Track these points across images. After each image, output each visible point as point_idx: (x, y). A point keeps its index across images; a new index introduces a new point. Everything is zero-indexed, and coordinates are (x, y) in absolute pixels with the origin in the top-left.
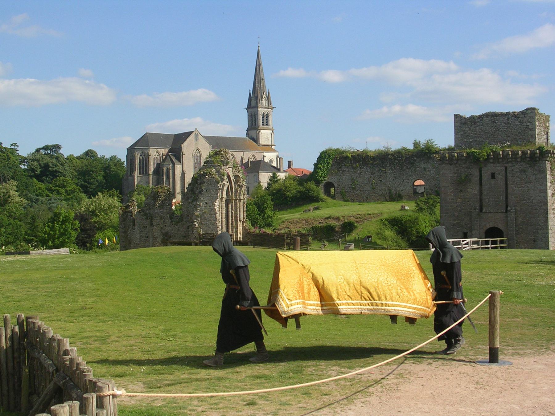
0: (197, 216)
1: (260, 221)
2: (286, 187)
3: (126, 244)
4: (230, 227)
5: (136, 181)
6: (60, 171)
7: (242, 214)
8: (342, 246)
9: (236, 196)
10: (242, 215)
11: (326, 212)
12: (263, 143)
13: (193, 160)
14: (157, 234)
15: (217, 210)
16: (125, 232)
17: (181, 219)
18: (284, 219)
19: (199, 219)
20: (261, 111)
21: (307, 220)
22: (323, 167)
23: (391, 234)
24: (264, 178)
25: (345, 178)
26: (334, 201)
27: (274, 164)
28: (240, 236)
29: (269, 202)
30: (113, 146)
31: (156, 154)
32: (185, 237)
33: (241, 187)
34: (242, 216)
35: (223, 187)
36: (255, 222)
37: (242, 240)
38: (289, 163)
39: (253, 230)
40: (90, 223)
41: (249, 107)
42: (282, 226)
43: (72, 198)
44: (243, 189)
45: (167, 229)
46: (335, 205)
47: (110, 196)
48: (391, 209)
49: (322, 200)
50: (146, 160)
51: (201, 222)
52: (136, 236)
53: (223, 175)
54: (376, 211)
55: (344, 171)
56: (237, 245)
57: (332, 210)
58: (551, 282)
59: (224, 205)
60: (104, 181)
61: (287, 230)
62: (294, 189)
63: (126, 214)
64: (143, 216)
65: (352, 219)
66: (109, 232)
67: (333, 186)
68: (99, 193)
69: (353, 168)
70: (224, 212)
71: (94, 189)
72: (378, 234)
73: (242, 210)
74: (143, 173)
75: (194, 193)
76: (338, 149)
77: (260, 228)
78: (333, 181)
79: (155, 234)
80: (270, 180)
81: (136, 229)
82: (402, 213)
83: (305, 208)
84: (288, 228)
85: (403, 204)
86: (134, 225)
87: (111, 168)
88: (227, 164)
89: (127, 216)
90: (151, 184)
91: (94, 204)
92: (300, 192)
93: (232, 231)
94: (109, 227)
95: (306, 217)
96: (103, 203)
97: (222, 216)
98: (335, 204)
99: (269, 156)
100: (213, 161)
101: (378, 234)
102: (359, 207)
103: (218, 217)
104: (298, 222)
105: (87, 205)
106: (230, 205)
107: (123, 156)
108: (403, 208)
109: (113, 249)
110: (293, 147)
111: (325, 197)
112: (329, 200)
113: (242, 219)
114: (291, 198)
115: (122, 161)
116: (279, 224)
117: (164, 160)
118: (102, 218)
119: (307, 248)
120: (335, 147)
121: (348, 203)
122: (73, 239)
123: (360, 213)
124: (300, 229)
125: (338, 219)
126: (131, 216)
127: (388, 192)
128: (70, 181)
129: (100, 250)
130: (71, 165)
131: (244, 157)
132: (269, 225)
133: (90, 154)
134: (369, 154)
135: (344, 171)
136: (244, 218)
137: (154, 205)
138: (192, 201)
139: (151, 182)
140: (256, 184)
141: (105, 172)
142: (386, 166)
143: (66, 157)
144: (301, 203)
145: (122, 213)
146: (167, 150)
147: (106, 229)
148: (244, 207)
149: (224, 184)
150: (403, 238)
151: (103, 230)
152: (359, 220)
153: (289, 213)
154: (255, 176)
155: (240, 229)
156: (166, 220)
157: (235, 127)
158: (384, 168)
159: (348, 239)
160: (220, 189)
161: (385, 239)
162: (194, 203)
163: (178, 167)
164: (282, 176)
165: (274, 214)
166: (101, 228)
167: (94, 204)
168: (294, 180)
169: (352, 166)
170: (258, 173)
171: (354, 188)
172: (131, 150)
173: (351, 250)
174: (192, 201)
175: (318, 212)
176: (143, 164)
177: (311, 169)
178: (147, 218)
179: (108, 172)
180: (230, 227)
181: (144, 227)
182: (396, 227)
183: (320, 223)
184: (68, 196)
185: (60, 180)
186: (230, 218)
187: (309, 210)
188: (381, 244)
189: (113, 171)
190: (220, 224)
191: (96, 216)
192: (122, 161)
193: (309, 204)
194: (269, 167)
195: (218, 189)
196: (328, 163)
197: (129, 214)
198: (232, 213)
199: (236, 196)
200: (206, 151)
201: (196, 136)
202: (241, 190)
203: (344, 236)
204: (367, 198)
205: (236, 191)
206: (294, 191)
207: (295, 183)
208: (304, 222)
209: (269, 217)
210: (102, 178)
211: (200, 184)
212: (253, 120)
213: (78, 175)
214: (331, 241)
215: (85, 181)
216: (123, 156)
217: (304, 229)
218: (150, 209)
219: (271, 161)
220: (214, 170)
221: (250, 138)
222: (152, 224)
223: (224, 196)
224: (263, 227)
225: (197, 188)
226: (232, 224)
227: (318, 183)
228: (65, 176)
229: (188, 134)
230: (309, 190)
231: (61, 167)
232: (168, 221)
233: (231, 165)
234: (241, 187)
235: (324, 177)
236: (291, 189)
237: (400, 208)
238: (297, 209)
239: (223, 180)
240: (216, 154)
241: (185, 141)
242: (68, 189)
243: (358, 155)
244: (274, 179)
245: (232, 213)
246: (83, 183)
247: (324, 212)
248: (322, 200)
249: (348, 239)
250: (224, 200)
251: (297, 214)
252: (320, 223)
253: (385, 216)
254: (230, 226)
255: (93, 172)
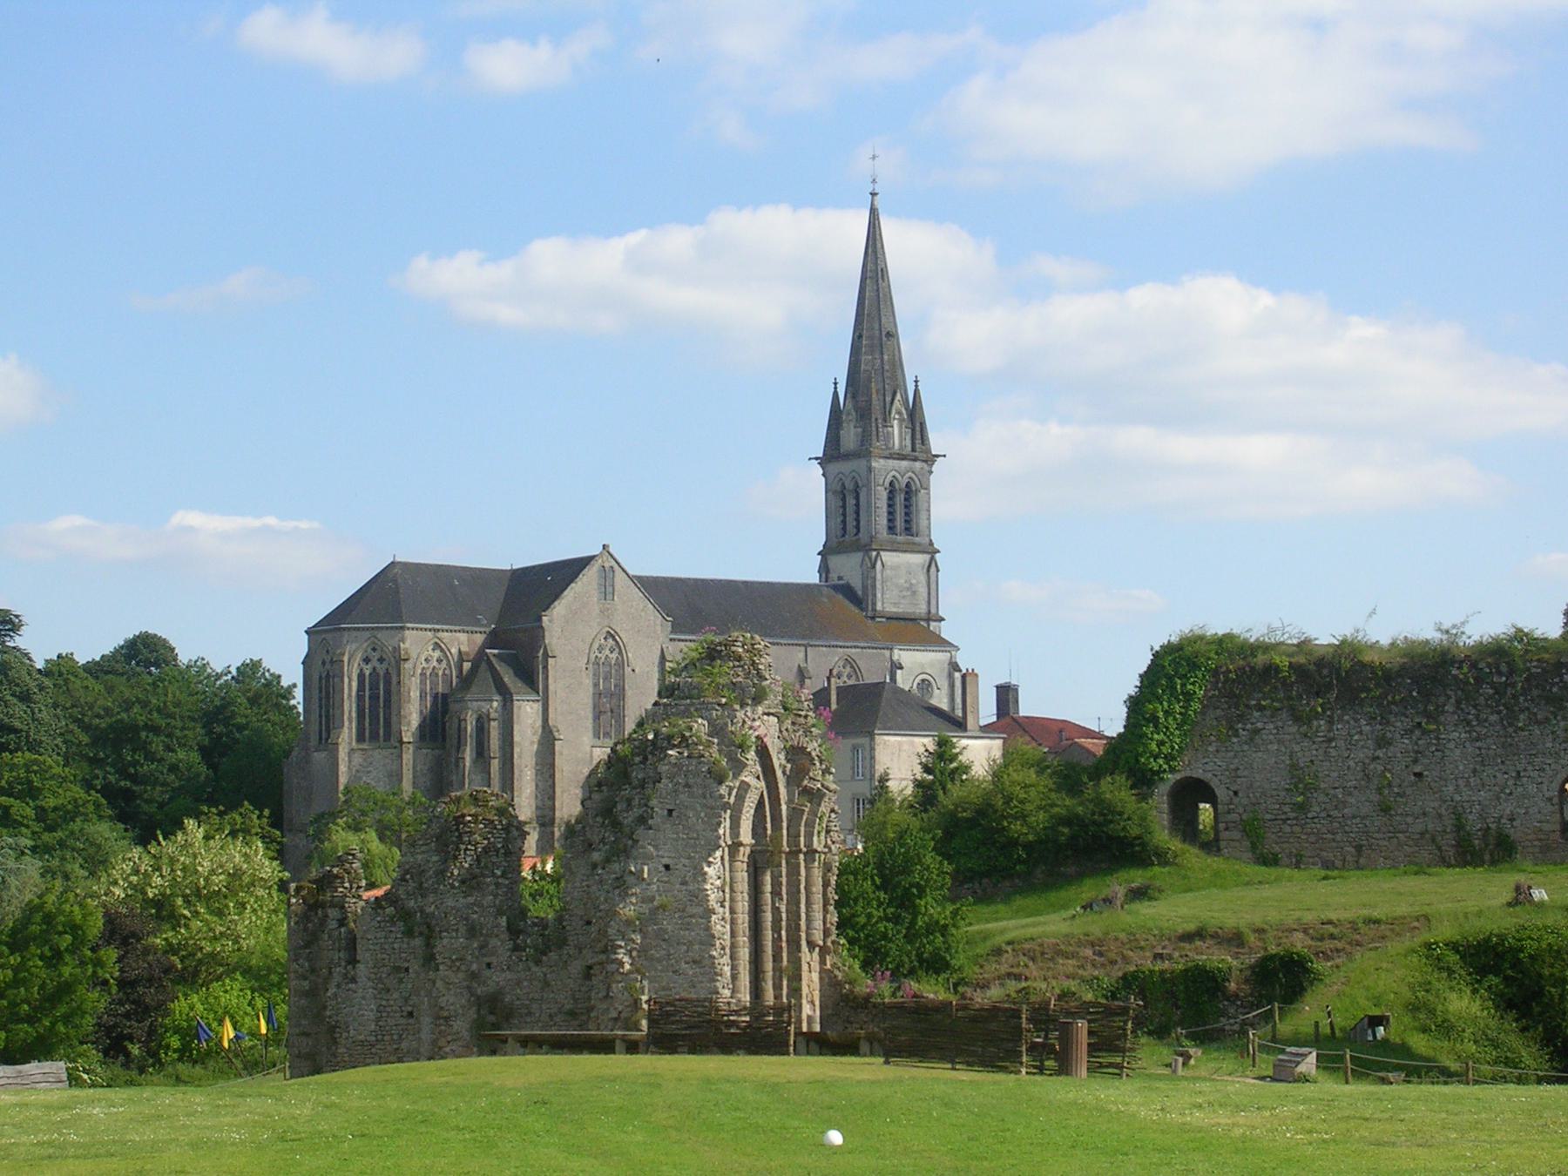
0: (629, 923)
1: (896, 947)
2: (1008, 800)
3: (315, 1047)
4: (769, 974)
5: (343, 768)
6: (17, 724)
7: (818, 916)
8: (1266, 1064)
9: (794, 837)
10: (819, 919)
11: (1184, 911)
12: (891, 609)
13: (588, 682)
14: (453, 1000)
15: (713, 897)
16: (313, 993)
17: (552, 939)
18: (999, 940)
19: (638, 938)
20: (885, 470)
21: (1101, 942)
22: (1167, 713)
23: (1475, 1008)
24: (900, 758)
25: (1260, 761)
26: (1215, 862)
27: (940, 700)
28: (810, 1011)
29: (930, 858)
30: (247, 616)
31: (428, 651)
32: (572, 1014)
33: (815, 796)
34: (818, 924)
35: (741, 798)
36: (876, 951)
37: (817, 1028)
38: (1006, 695)
39: (865, 985)
40: (147, 951)
41: (833, 454)
42: (992, 968)
43: (62, 844)
44: (824, 808)
45: (497, 979)
46: (1217, 880)
47: (233, 834)
48: (1474, 900)
49: (1162, 857)
50: (388, 683)
51: (643, 950)
52: (360, 1007)
53: (743, 747)
54: (1402, 909)
55: (1257, 731)
56: (808, 1053)
57: (1206, 904)
58: (8, 1098)
59: (743, 876)
60: (203, 769)
61: (1013, 986)
62: (1039, 807)
63: (315, 907)
64: (392, 920)
65: (1300, 944)
66: (232, 993)
67: (1211, 798)
68: (190, 823)
69: (1297, 719)
70: (743, 905)
71: (161, 806)
72: (1414, 1008)
73: (818, 898)
74: (374, 736)
75: (616, 825)
76: (1229, 637)
77: (896, 975)
78: (1207, 777)
79: (442, 1001)
80: (927, 769)
81: (362, 980)
82: (1522, 916)
83: (1088, 889)
84: (1018, 977)
85: (1521, 878)
86: (353, 961)
87: (234, 714)
88: (758, 699)
89: (324, 921)
90: (407, 785)
91: (166, 870)
92: (1068, 821)
93: (777, 987)
94: (230, 971)
95: (1096, 930)
96: (204, 867)
97: (733, 922)
98: (1216, 874)
99: (914, 664)
100: (698, 687)
101: (1414, 1008)
102: (1324, 888)
103: (720, 928)
104: (1060, 953)
105: (136, 872)
106: (768, 878)
107: (287, 664)
108: (1521, 897)
109: (254, 1066)
110: (1045, 630)
111: (1175, 845)
112: (1192, 857)
113: (818, 937)
114: (1028, 846)
115: (285, 683)
116: (977, 960)
117: (466, 681)
118: (198, 927)
119: (1120, 1067)
120: (1217, 627)
121: (1272, 872)
122: (89, 1022)
123: (1333, 916)
124: (1073, 985)
125: (1235, 939)
126: (342, 922)
127: (1449, 822)
128: (57, 770)
129: (198, 1069)
130: (61, 700)
131: (811, 667)
132: (936, 965)
133: (145, 652)
134: (1367, 658)
135: (1257, 731)
136: (826, 933)
137: (441, 873)
138: (608, 860)
139: (407, 776)
140: (864, 789)
141: (210, 732)
142: (1440, 710)
143: (40, 665)
144: (1071, 870)
145: (299, 910)
146: (480, 639)
147: (219, 978)
148: (826, 884)
149: (745, 787)
150: (1524, 1030)
151: (206, 984)
152: (1328, 945)
153: (1017, 914)
154: (855, 748)
155: (811, 982)
156: (494, 942)
157: (779, 538)
158: (1430, 717)
159: (1285, 1028)
160: (726, 806)
161: (1446, 1029)
162: (616, 867)
163: (527, 712)
164: (979, 754)
165: (955, 913)
166: (195, 971)
167: (166, 870)
168: (1040, 772)
169: (1292, 709)
170: (872, 736)
171: (1302, 808)
172: (325, 637)
173: (1305, 1079)
174: (608, 860)
175: (1145, 911)
176: (374, 697)
177: (1114, 724)
178: (409, 933)
179: (219, 729)
180: (769, 974)
181: (397, 969)
182: (1494, 980)
183: (1158, 957)
184: (46, 837)
185: (13, 767)
186: (768, 935)
187: (1108, 901)
188: (1431, 1053)
189: (241, 728)
190: (726, 959)
191: (174, 920)
192: (285, 683)
193: (1110, 871)
194: (917, 711)
195: (715, 809)
196: (1189, 696)
197: (333, 913)
198: (776, 911)
199: (794, 837)
200: (650, 647)
201: (607, 575)
202: (814, 813)
203: (1268, 1017)
204: (1359, 848)
205: (795, 814)
206: (1042, 815)
207: (1046, 781)
208: (1089, 952)
209: (934, 927)
210: (195, 757)
211: (643, 785)
212: (850, 509)
213: (95, 742)
214: (1206, 1038)
215: (123, 773)
216: (287, 664)
217: (1089, 982)
218: (422, 891)
219: (925, 685)
220: (700, 726)
221: (836, 588)
222: (429, 960)
223: (746, 836)
224: (912, 972)
225: (629, 801)
226: (777, 957)
227: (1143, 781)
228: (34, 746)
229: (570, 570)
230: (1108, 812)
231: (19, 709)
232: (501, 945)
233: (773, 701)
234: (815, 796)
235: (1169, 758)
236: (1029, 807)
237: (1508, 896)
238: (1053, 896)
239: (739, 767)
240: (712, 654)
241: (557, 596)
242: (51, 802)
243: (1321, 663)
244: (942, 764)
245: (776, 911)
246: (112, 778)
247: (1173, 911)
248: (1162, 857)
249: (1285, 1028)
250: (743, 854)
251: (1053, 917)
252: (1158, 957)
253: (1446, 931)
254: (769, 966)
255: (155, 730)
